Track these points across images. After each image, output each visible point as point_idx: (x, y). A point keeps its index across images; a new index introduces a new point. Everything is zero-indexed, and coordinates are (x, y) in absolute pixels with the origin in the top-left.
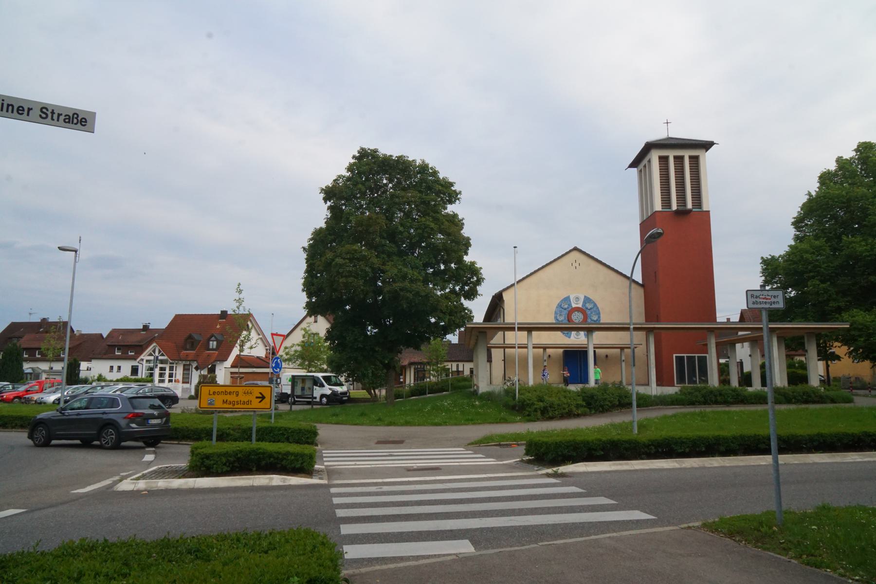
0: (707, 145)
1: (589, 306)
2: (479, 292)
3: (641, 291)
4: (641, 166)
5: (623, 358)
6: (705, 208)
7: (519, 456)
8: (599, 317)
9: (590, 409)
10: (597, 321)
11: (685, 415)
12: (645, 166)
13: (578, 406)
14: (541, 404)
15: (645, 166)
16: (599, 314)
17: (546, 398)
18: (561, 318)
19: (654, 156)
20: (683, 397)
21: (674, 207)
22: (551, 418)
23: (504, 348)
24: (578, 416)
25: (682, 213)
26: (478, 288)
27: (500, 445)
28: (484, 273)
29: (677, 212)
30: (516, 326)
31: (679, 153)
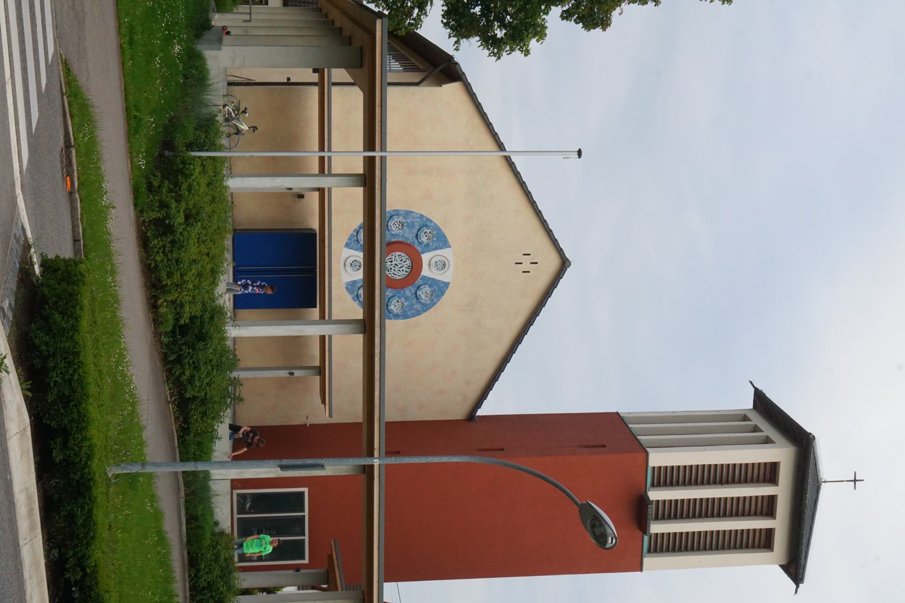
0: (795, 568)
1: (424, 293)
2: (464, 42)
3: (458, 412)
4: (757, 420)
5: (297, 373)
6: (648, 561)
7: (38, 238)
8: (397, 316)
9: (173, 332)
10: (387, 313)
11: (164, 562)
12: (756, 429)
13: (177, 305)
14: (181, 219)
15: (756, 429)
16: (405, 316)
17: (197, 228)
18: (394, 227)
19: (780, 453)
20: (207, 542)
21: (655, 495)
22: (144, 243)
23: (321, 84)
24: (153, 306)
25: (640, 512)
26: (475, 41)
27: (68, 146)
28: (513, 59)
29: (642, 502)
30: (377, 154)
31: (783, 508)
